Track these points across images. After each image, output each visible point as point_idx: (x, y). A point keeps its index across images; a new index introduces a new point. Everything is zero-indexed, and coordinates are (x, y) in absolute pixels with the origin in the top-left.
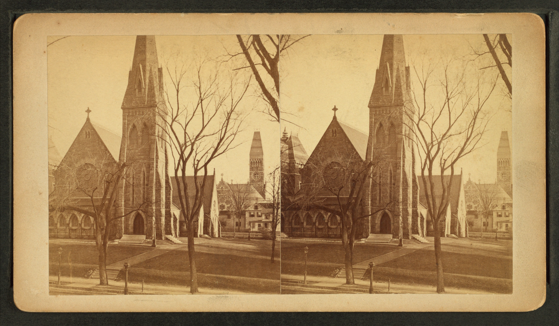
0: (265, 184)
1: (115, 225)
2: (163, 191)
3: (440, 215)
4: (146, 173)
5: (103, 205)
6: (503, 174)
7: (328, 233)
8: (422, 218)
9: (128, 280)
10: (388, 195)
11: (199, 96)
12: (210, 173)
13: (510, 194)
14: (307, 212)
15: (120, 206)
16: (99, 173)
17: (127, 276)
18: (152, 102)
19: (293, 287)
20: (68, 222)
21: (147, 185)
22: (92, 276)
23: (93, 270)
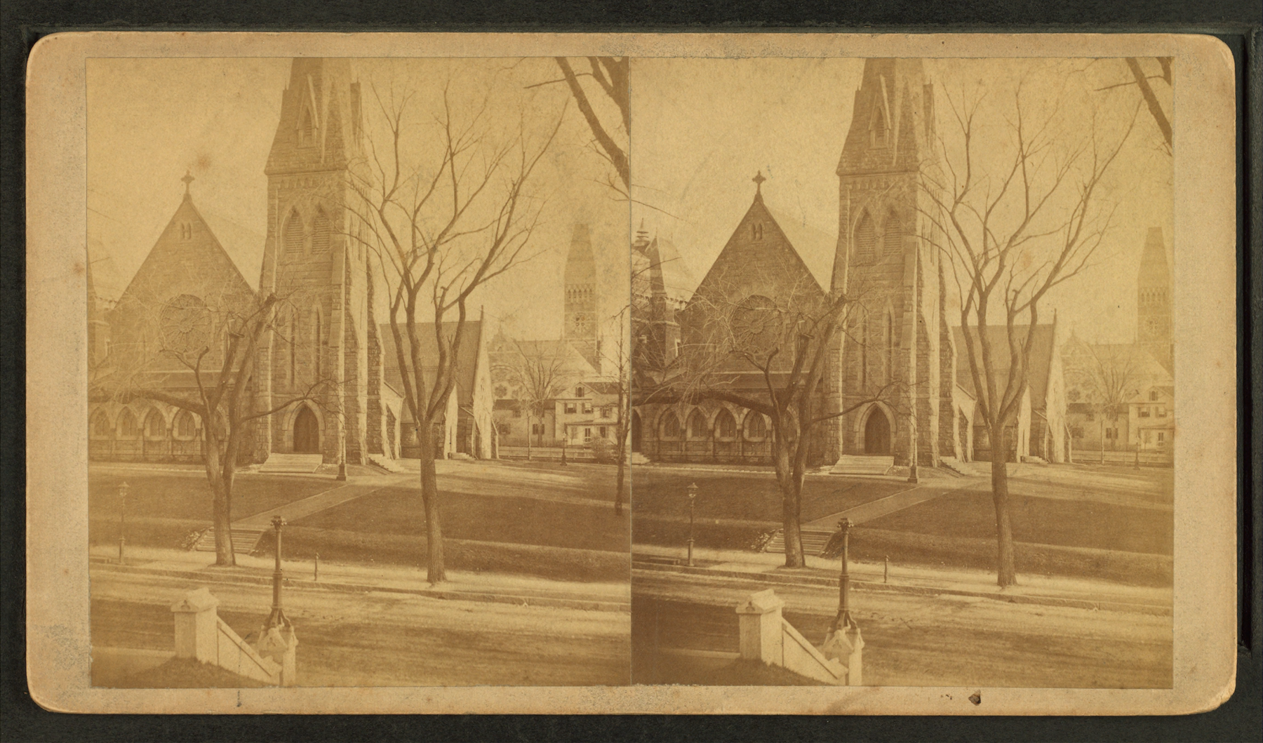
0: (600, 339)
1: (250, 433)
2: (363, 354)
3: (434, 410)
4: (321, 316)
5: (223, 387)
6: (578, 319)
7: (743, 453)
8: (963, 419)
9: (282, 554)
10: (883, 368)
11: (447, 144)
12: (472, 316)
13: (1171, 369)
14: (693, 407)
15: (262, 391)
16: (213, 315)
17: (280, 547)
18: (337, 159)
19: (661, 572)
20: (140, 426)
21: (897, 344)
22: (769, 547)
23: (201, 533)
